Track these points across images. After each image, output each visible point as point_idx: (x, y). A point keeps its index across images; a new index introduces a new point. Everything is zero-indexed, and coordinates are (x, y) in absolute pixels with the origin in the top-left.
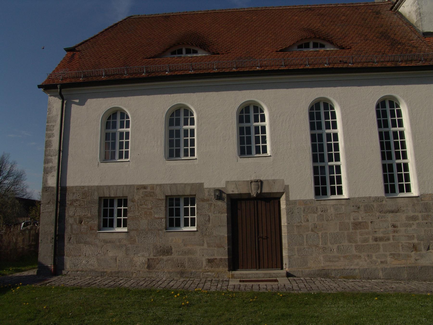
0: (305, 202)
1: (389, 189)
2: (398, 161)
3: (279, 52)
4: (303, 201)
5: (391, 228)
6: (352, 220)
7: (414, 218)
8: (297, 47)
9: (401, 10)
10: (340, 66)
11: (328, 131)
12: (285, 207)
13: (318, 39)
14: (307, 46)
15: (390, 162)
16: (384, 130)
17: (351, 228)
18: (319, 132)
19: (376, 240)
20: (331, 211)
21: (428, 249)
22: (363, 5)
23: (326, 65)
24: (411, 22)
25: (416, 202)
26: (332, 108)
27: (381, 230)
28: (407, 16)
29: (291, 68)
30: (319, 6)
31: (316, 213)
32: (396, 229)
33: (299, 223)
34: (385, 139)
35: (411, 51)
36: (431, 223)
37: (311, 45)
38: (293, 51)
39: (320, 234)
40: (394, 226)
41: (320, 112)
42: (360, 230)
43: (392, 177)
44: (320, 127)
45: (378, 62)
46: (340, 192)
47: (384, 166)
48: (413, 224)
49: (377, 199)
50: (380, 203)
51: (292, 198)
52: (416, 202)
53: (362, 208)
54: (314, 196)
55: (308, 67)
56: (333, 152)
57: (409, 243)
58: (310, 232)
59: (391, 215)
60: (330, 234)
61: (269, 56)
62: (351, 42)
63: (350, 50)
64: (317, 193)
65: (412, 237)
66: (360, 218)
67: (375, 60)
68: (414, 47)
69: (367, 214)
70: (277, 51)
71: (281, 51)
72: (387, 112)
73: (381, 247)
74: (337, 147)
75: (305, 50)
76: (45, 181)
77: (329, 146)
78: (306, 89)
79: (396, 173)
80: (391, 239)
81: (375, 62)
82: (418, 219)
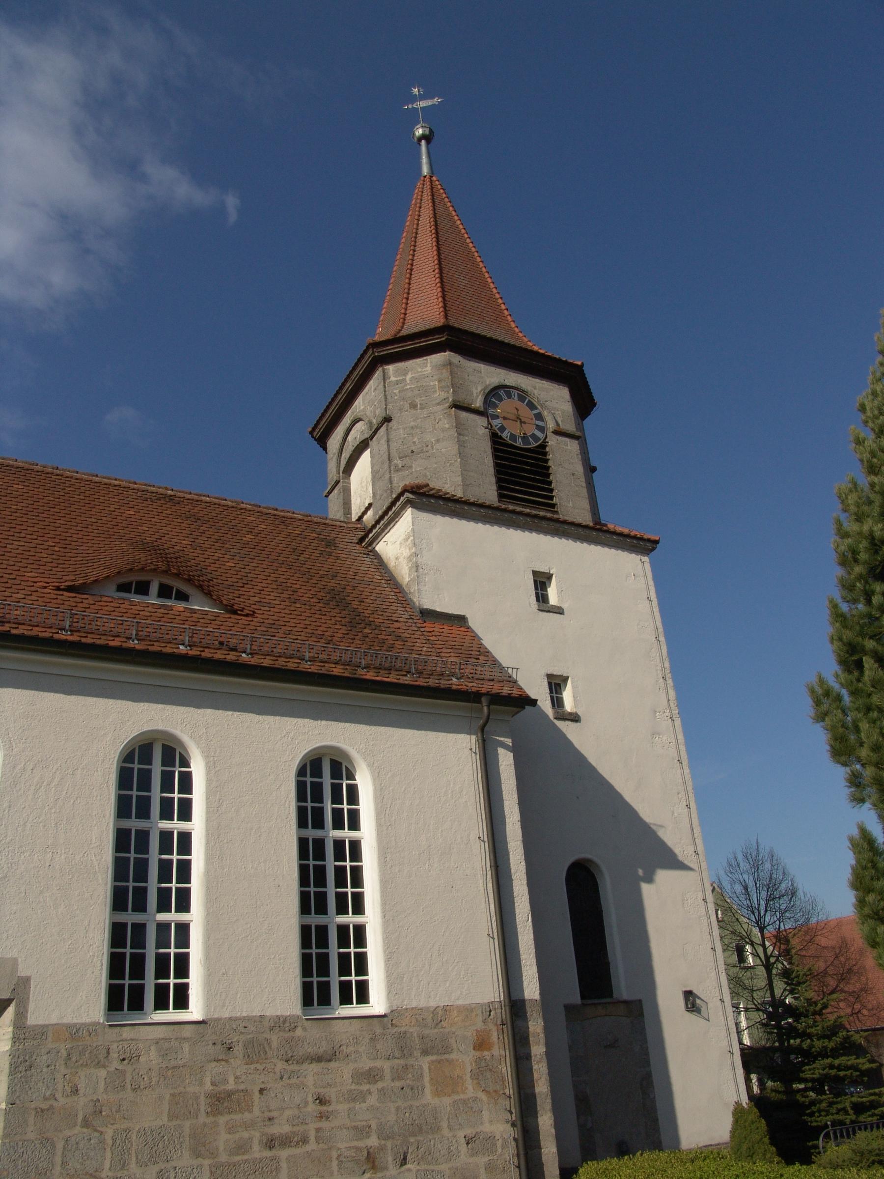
0: (74, 1032)
1: (315, 995)
2: (341, 919)
3: (63, 590)
4: (69, 1026)
5: (313, 1108)
6: (208, 1087)
7: (372, 1076)
8: (114, 587)
9: (380, 547)
10: (219, 655)
11: (165, 825)
12: (8, 1048)
13: (176, 580)
14: (143, 589)
15: (320, 920)
16: (311, 833)
17: (202, 1108)
18: (142, 824)
19: (270, 1144)
20: (151, 1058)
21: (404, 1162)
22: (300, 517)
23: (181, 647)
24: (399, 579)
25: (379, 1030)
26: (185, 763)
27: (288, 1113)
28: (391, 564)
29: (89, 640)
30: (196, 497)
31: (104, 1066)
32: (324, 1108)
33: (46, 1099)
34: (314, 859)
35: (392, 647)
36: (412, 1089)
37: (154, 589)
38: (102, 596)
39: (109, 1133)
40: (321, 1101)
41: (150, 771)
42: (227, 1117)
43: (324, 960)
44: (144, 812)
45: (313, 660)
46: (182, 1002)
47: (305, 931)
48: (370, 1093)
49: (281, 1023)
50: (287, 1035)
51: (34, 1018)
52: (379, 1030)
53: (238, 1049)
54: (102, 1013)
55: (134, 644)
56: (174, 885)
57: (358, 1149)
58: (77, 1129)
59: (315, 1067)
60: (139, 1132)
61: (33, 598)
62: (256, 599)
63: (250, 619)
64: (115, 1002)
65: (362, 1131)
66: (231, 1080)
67: (307, 655)
68: (398, 638)
69: (253, 1067)
70: (58, 588)
71: (70, 589)
72: (322, 788)
73: (284, 1165)
74: (185, 870)
75: (136, 598)
76: (741, 1042)
77: (165, 869)
78: (119, 702)
79: (334, 950)
80: (312, 1139)
81: (307, 658)
82: (382, 1078)
